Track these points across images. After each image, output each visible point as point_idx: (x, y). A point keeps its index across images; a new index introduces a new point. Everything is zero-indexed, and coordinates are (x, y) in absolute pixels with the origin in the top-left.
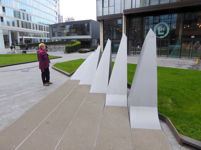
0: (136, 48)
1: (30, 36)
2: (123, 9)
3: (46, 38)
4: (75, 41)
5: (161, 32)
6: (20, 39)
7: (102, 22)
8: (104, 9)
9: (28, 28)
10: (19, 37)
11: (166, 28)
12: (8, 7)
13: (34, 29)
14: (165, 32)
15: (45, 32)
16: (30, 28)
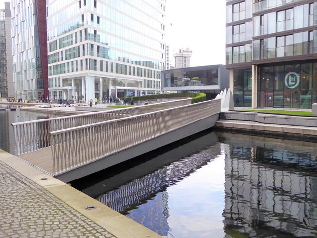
3: (146, 89)
4: (195, 92)
5: (292, 82)
6: (112, 89)
9: (92, 70)
10: (111, 88)
11: (296, 79)
13: (130, 74)
14: (296, 82)
15: (145, 78)
16: (126, 74)
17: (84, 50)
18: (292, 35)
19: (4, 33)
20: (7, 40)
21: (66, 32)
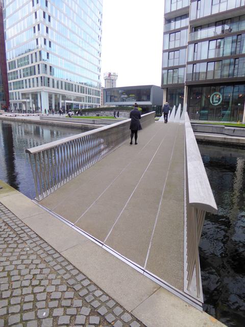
0: (222, 109)
1: (71, 100)
2: (186, 61)
7: (166, 90)
8: (170, 61)
10: (61, 101)
12: (54, 42)
15: (86, 95)
16: (72, 91)
17: (39, 69)
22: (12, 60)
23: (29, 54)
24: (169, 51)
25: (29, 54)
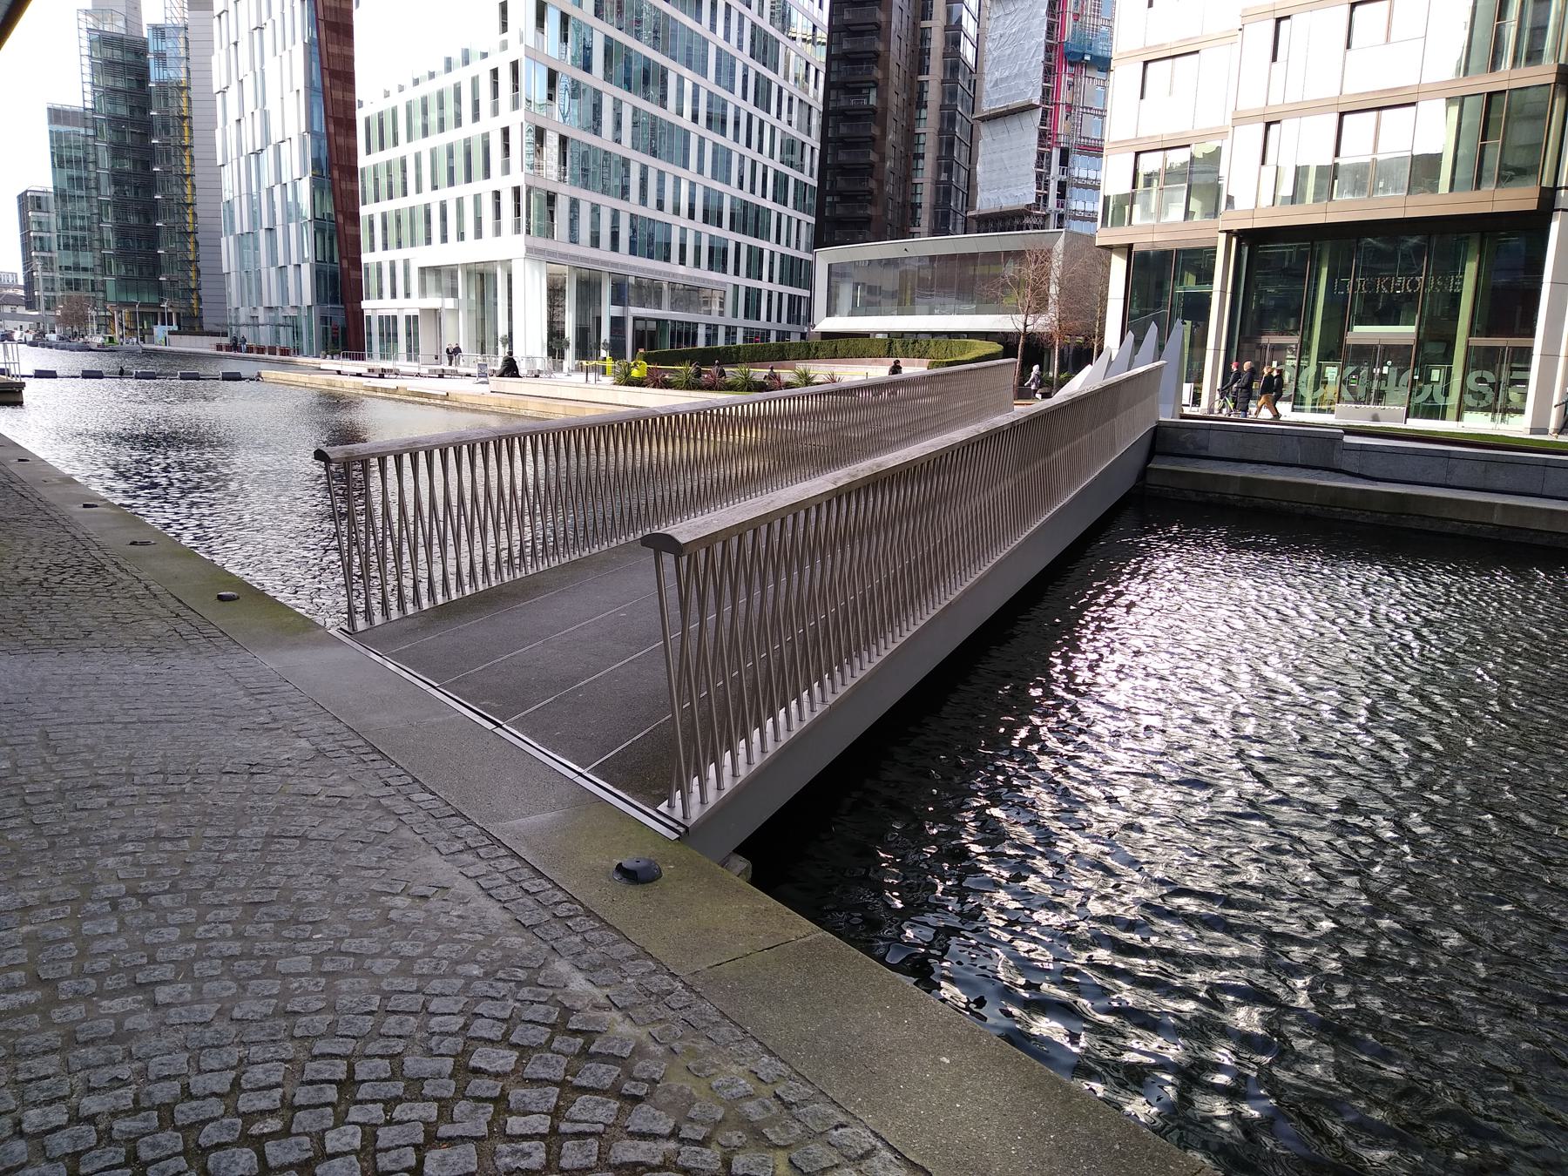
16: (667, 259)
17: (507, 148)
18: (1413, 109)
19: (183, 75)
20: (194, 104)
21: (422, 404)
22: (385, 106)
23: (462, 75)
24: (654, 124)
25: (462, 75)
